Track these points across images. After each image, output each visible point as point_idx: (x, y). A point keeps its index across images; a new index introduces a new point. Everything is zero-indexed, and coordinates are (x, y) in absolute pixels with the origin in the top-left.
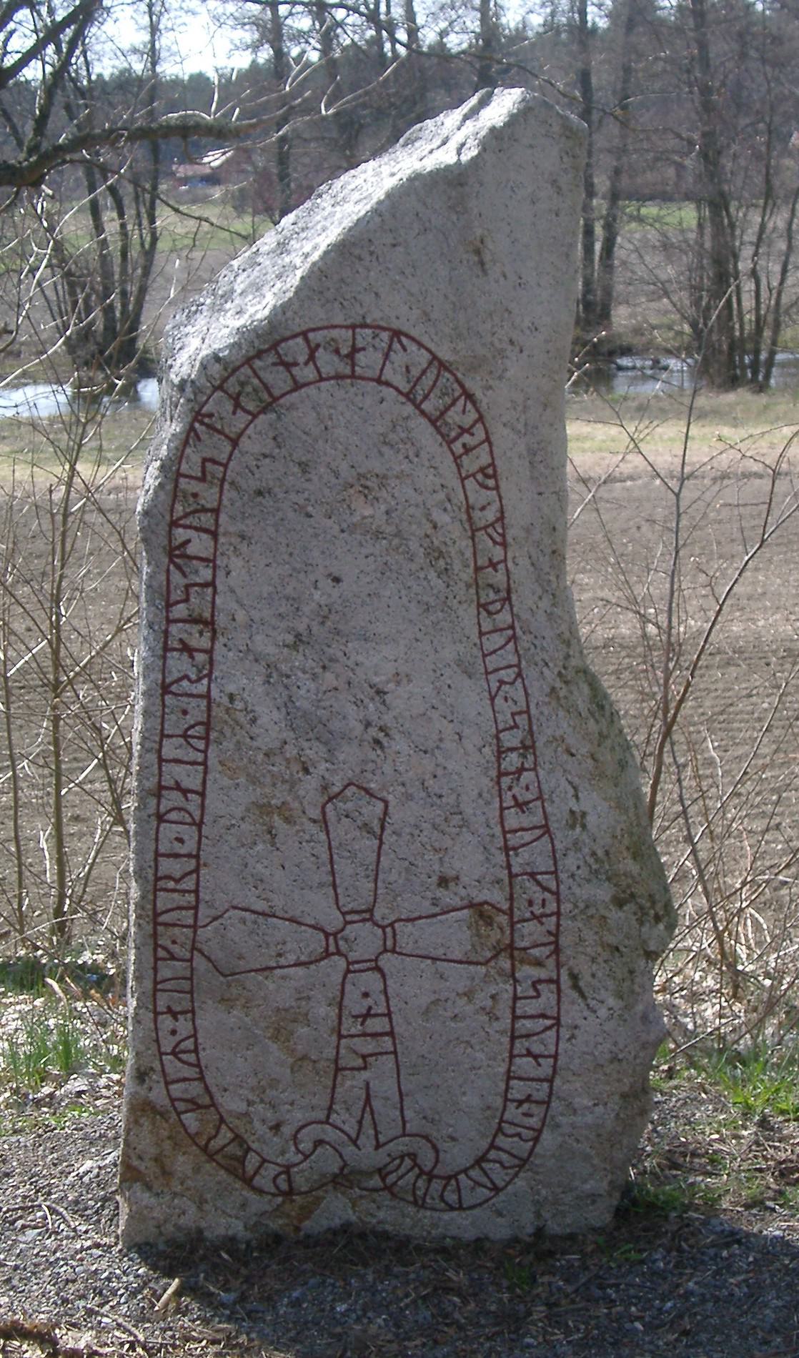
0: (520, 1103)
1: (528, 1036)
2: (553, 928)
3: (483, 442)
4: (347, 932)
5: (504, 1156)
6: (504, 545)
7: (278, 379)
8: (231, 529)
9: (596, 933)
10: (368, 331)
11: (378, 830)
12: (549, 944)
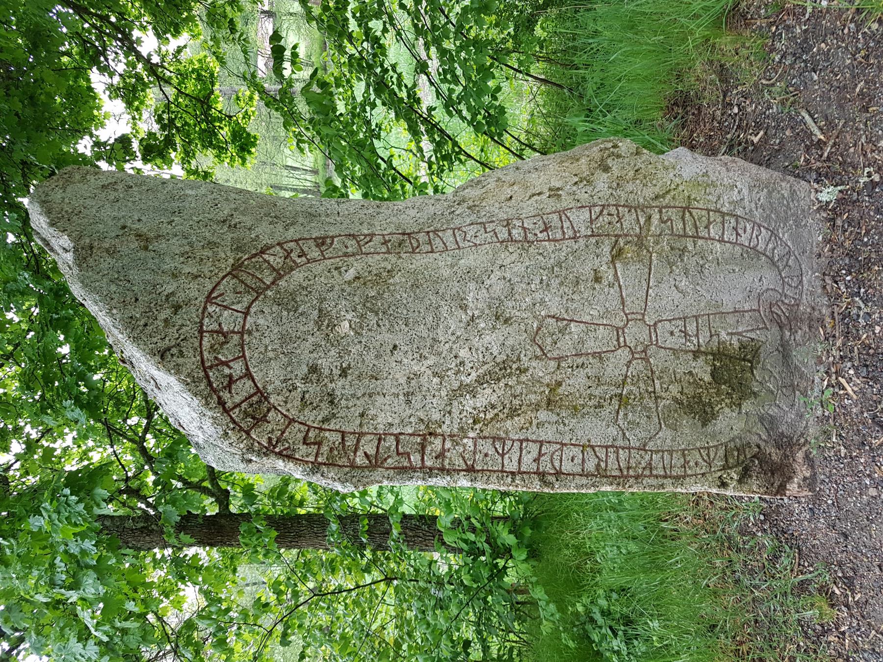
0: (738, 234)
1: (696, 228)
2: (626, 210)
3: (298, 244)
4: (632, 345)
5: (770, 246)
6: (372, 235)
7: (244, 388)
8: (358, 422)
9: (628, 182)
10: (206, 320)
11: (565, 322)
12: (636, 212)
